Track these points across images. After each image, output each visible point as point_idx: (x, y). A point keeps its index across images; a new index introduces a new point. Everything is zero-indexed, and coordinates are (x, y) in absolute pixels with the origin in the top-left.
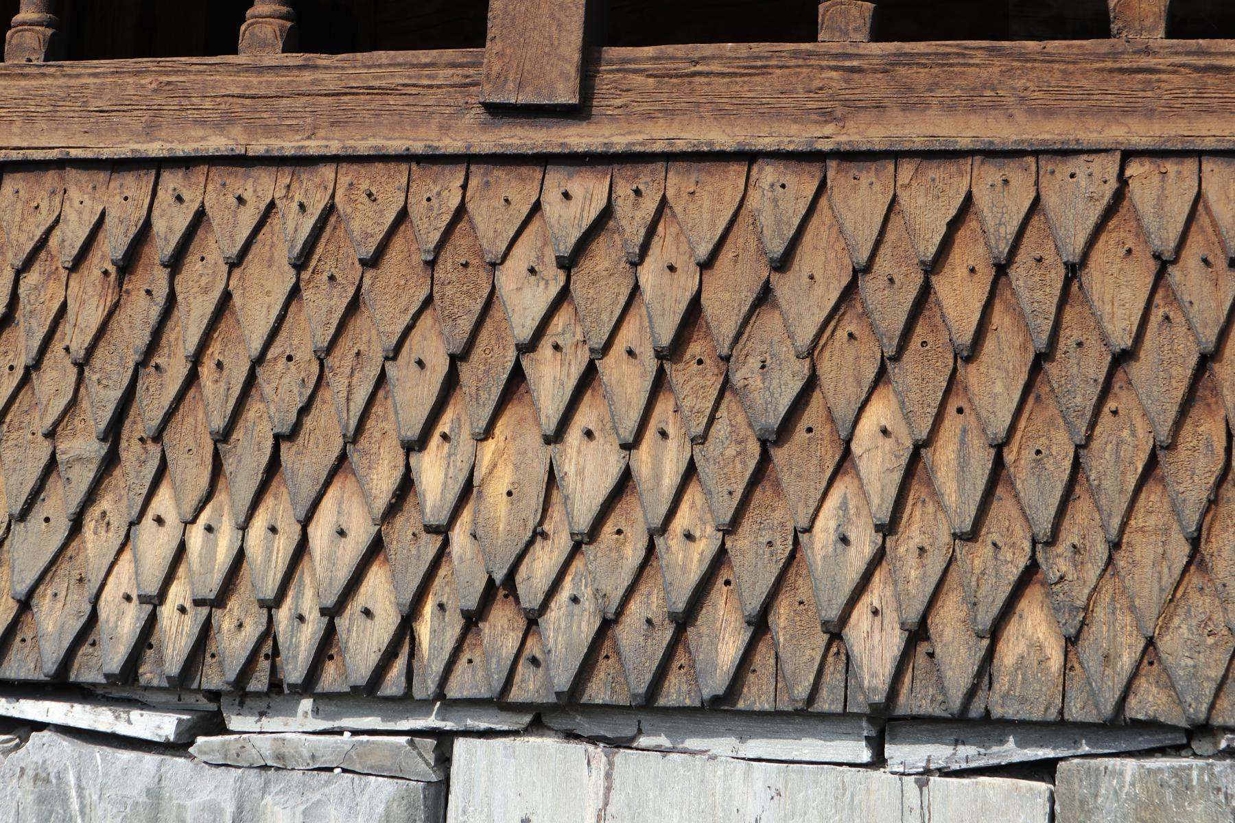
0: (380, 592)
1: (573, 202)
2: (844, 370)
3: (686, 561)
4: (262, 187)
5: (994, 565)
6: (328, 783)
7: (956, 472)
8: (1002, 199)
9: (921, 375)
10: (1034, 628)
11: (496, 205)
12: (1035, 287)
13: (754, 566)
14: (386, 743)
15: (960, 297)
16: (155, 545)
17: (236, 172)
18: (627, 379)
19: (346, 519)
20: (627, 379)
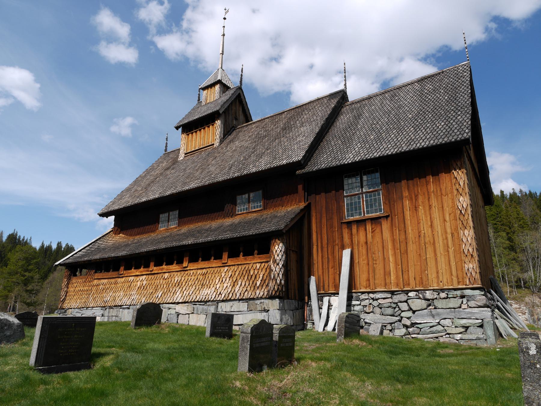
0: (215, 294)
1: (226, 268)
2: (238, 278)
3: (229, 290)
4: (211, 269)
5: (245, 289)
6: (352, 125)
7: (243, 285)
8: (247, 266)
9: (242, 278)
10: (246, 293)
11: (222, 269)
12: (248, 272)
13: (233, 291)
14: (478, 168)
15: (244, 272)
16: (203, 292)
17: (190, 22)
18: (228, 279)
19: (213, 289)
20: (228, 279)
